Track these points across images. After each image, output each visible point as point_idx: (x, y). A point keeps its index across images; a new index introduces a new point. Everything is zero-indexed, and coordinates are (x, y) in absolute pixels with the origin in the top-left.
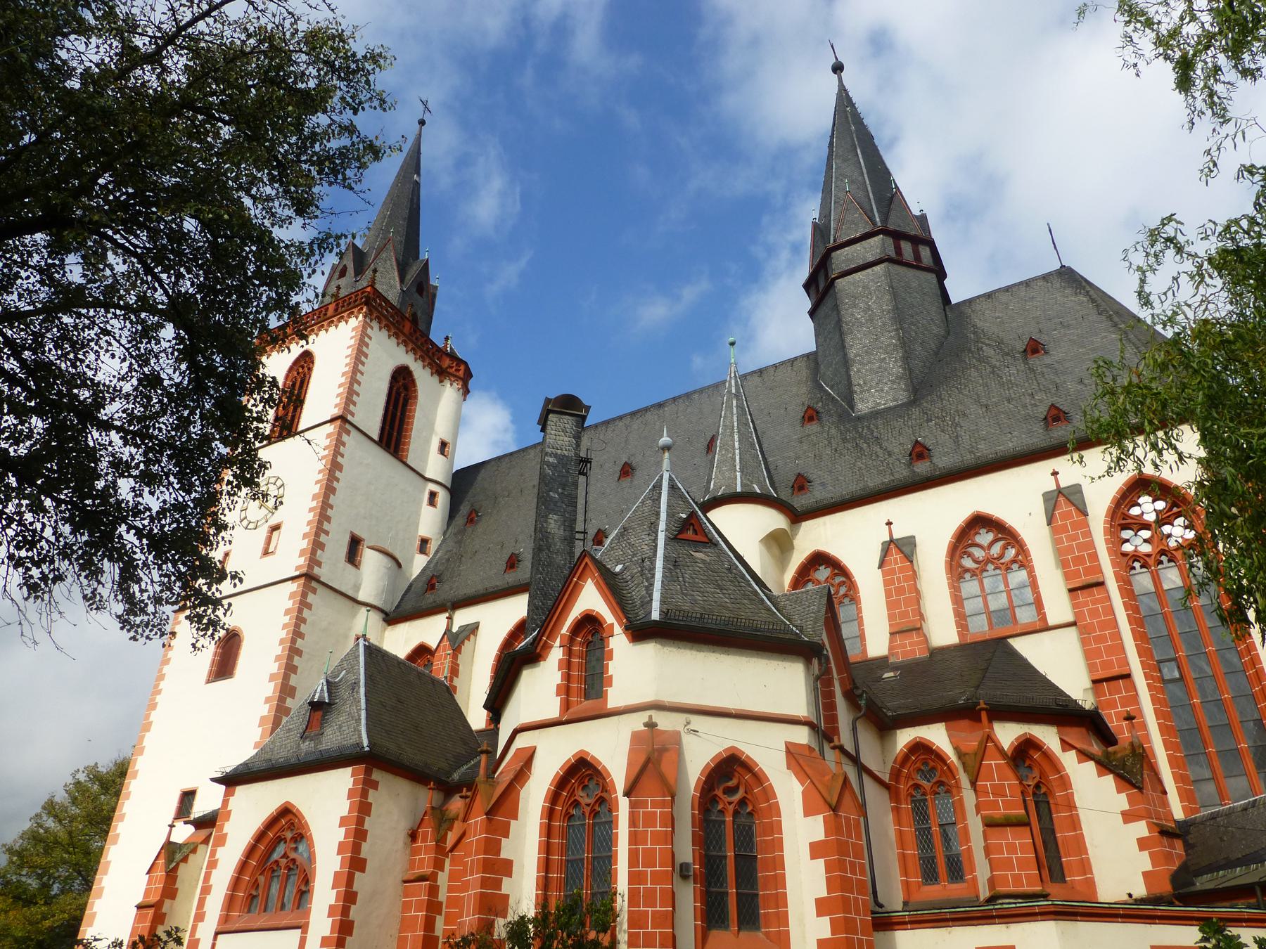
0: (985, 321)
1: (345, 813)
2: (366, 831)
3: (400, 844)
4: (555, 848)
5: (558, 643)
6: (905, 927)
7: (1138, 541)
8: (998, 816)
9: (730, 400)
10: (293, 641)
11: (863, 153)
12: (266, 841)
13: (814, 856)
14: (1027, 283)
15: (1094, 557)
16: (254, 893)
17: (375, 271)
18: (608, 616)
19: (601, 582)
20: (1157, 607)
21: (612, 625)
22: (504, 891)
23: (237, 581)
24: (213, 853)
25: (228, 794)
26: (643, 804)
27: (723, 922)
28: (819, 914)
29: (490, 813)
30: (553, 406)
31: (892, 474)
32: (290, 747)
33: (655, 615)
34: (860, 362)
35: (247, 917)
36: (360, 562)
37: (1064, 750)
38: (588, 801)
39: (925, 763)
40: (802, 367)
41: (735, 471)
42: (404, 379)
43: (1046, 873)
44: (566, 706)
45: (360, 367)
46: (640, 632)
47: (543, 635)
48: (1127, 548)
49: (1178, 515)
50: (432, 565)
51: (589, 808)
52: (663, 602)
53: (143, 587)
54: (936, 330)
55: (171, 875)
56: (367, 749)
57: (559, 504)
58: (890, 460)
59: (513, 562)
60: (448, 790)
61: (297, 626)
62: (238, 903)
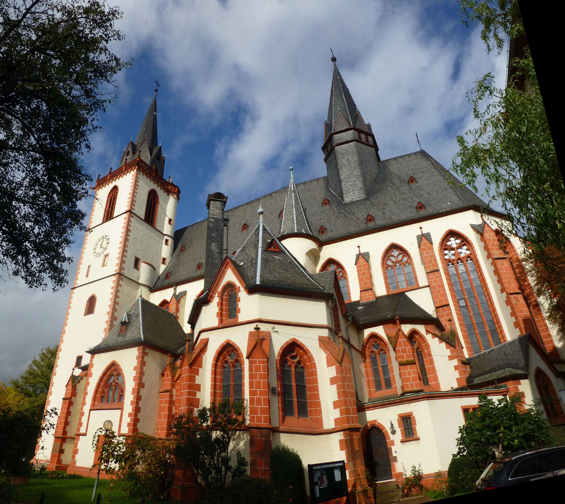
0: (393, 168)
2: (144, 372)
3: (158, 378)
4: (218, 380)
5: (217, 295)
7: (450, 254)
8: (404, 361)
10: (115, 299)
12: (107, 375)
14: (409, 155)
15: (435, 260)
16: (103, 395)
17: (140, 152)
18: (238, 283)
19: (234, 268)
20: (467, 277)
22: (197, 397)
24: (88, 380)
25: (92, 357)
26: (255, 362)
27: (291, 413)
28: (335, 408)
29: (191, 365)
31: (359, 227)
32: (116, 339)
33: (258, 282)
34: (346, 181)
35: (101, 404)
37: (427, 334)
38: (231, 361)
39: (375, 342)
40: (322, 184)
41: (294, 223)
43: (422, 382)
44: (221, 321)
45: (136, 190)
46: (252, 290)
48: (447, 257)
49: (464, 245)
51: (232, 364)
52: (261, 277)
54: (375, 170)
55: (74, 388)
58: (359, 221)
59: (199, 266)
60: (176, 357)
61: (116, 293)
62: (97, 399)
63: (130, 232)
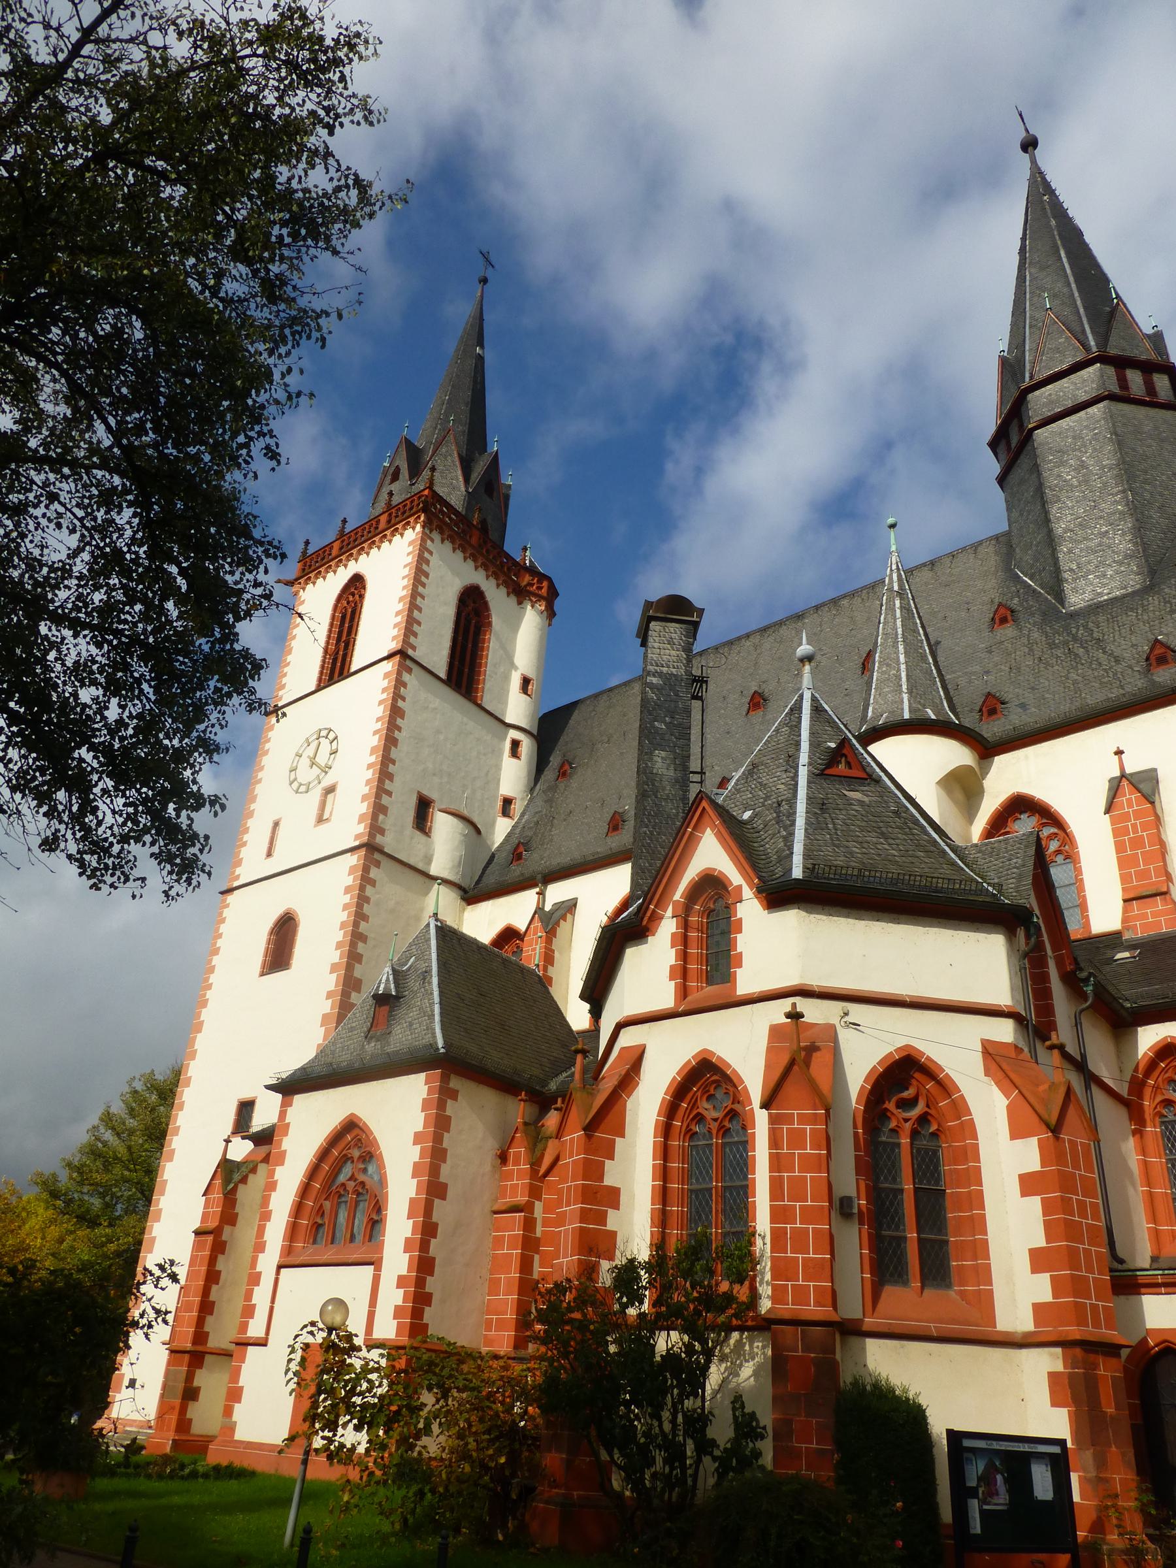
1: (420, 1127)
3: (488, 1167)
4: (674, 1175)
5: (669, 912)
6: (1157, 1290)
9: (890, 601)
10: (356, 924)
11: (1067, 253)
12: (330, 1160)
13: (1025, 1193)
17: (433, 469)
18: (734, 876)
19: (723, 831)
21: (740, 887)
22: (611, 1226)
23: (217, 807)
24: (272, 1173)
25: (286, 1104)
26: (789, 1119)
28: (1035, 1270)
29: (590, 1128)
30: (656, 611)
31: (1122, 687)
33: (797, 873)
35: (312, 1249)
36: (430, 828)
38: (715, 1114)
41: (901, 692)
44: (683, 992)
45: (420, 589)
47: (650, 903)
50: (518, 831)
52: (807, 856)
53: (101, 818)
55: (230, 1199)
56: (442, 1051)
58: (1119, 668)
59: (615, 824)
60: (543, 1102)
61: (359, 906)
62: (301, 1233)
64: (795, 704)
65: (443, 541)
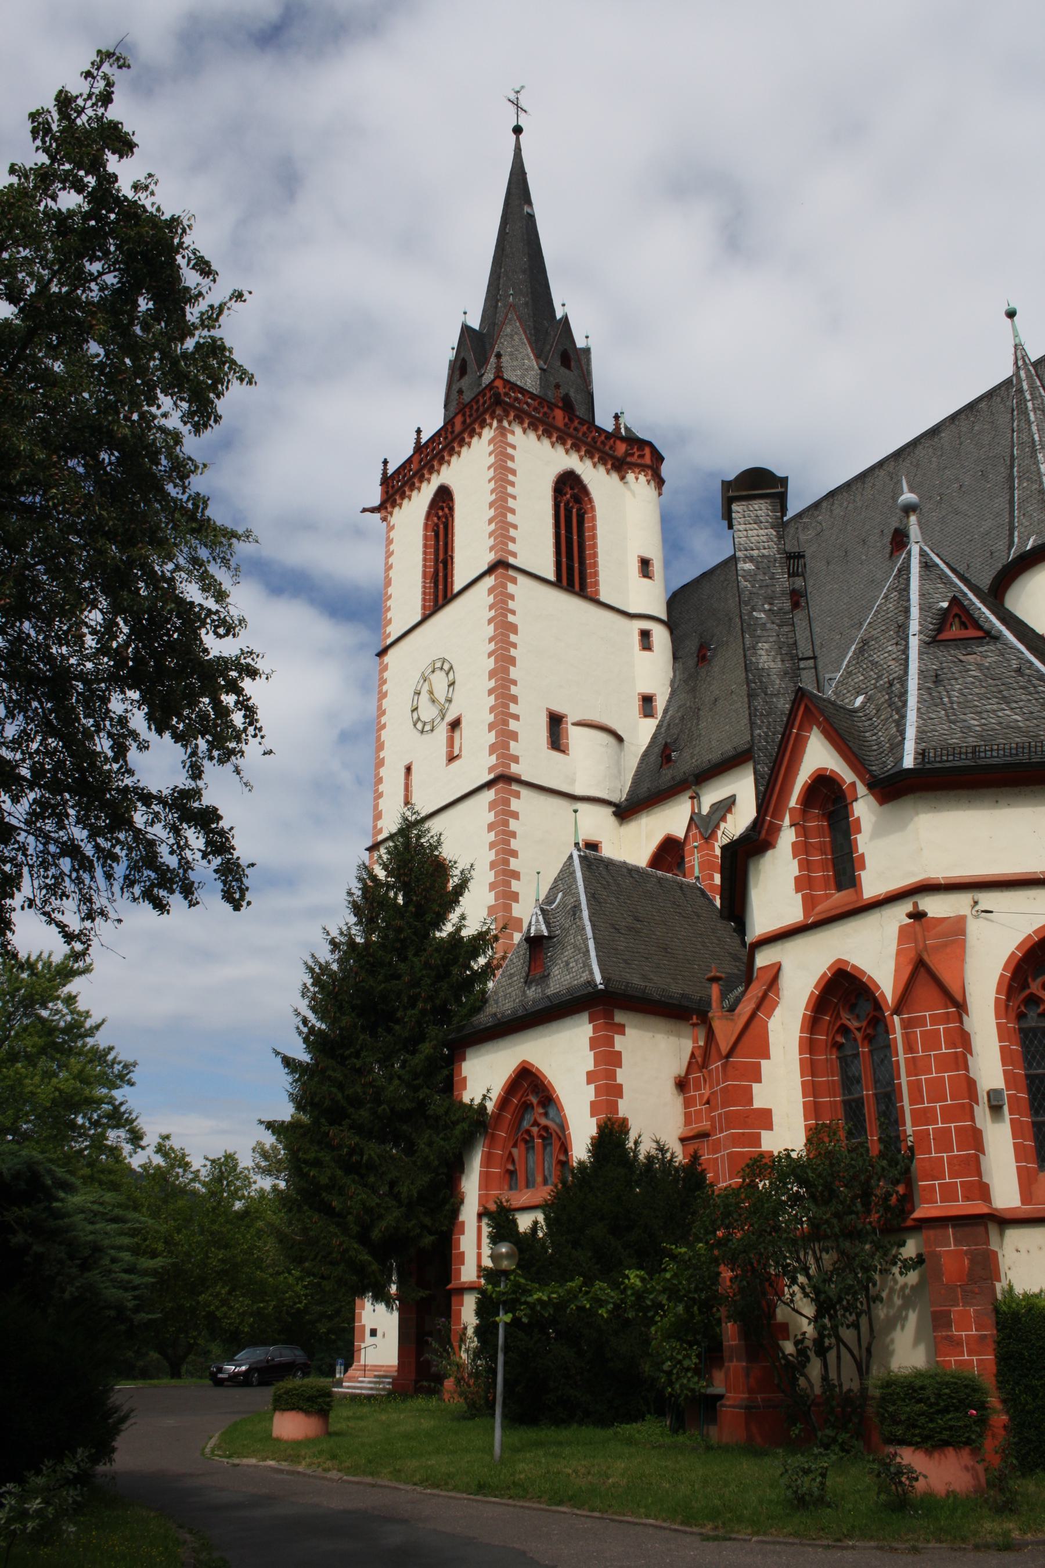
5: (787, 821)
17: (499, 356)
18: (847, 776)
26: (921, 1022)
33: (909, 762)
38: (856, 1024)
42: (571, 489)
44: (809, 903)
45: (510, 490)
50: (663, 730)
52: (919, 740)
57: (769, 626)
63: (516, 633)
64: (903, 563)
65: (524, 431)
